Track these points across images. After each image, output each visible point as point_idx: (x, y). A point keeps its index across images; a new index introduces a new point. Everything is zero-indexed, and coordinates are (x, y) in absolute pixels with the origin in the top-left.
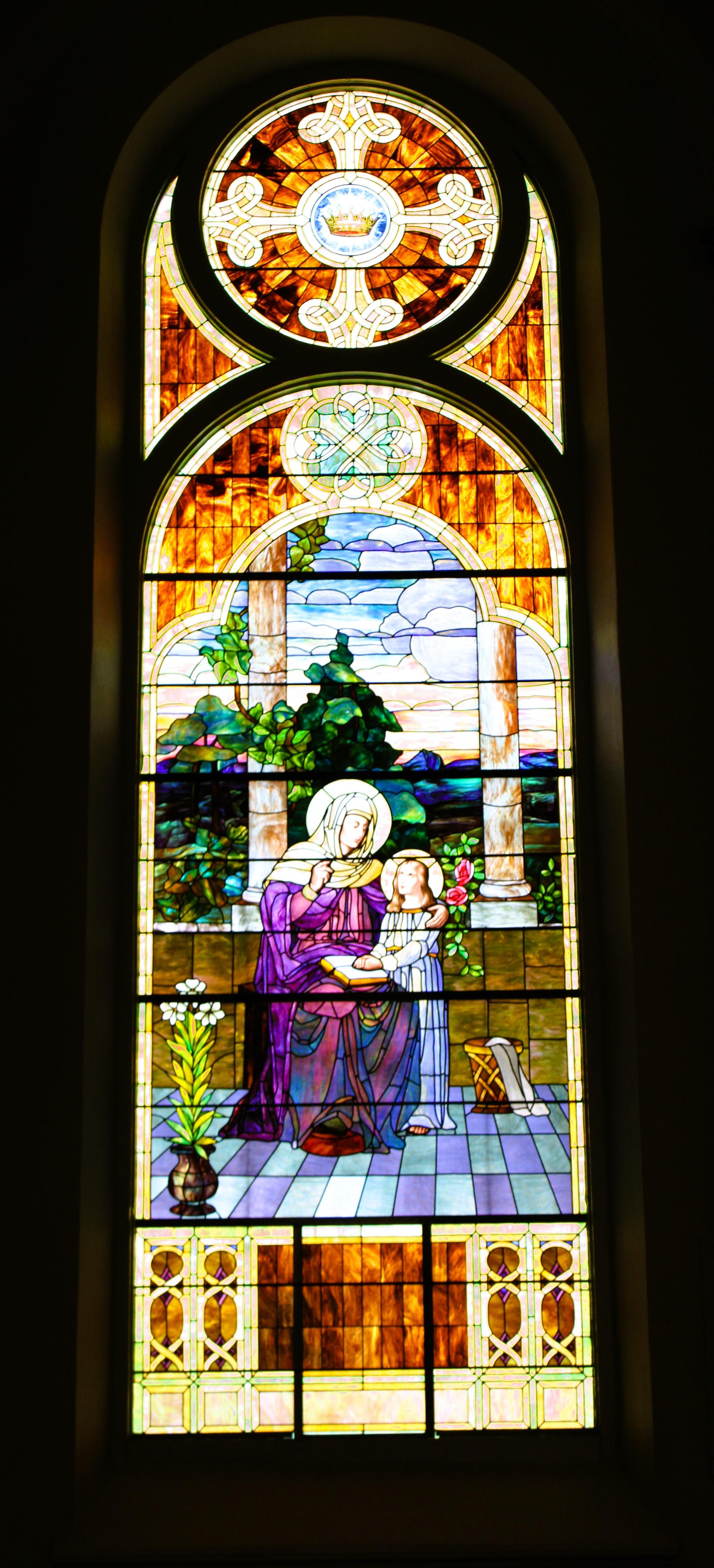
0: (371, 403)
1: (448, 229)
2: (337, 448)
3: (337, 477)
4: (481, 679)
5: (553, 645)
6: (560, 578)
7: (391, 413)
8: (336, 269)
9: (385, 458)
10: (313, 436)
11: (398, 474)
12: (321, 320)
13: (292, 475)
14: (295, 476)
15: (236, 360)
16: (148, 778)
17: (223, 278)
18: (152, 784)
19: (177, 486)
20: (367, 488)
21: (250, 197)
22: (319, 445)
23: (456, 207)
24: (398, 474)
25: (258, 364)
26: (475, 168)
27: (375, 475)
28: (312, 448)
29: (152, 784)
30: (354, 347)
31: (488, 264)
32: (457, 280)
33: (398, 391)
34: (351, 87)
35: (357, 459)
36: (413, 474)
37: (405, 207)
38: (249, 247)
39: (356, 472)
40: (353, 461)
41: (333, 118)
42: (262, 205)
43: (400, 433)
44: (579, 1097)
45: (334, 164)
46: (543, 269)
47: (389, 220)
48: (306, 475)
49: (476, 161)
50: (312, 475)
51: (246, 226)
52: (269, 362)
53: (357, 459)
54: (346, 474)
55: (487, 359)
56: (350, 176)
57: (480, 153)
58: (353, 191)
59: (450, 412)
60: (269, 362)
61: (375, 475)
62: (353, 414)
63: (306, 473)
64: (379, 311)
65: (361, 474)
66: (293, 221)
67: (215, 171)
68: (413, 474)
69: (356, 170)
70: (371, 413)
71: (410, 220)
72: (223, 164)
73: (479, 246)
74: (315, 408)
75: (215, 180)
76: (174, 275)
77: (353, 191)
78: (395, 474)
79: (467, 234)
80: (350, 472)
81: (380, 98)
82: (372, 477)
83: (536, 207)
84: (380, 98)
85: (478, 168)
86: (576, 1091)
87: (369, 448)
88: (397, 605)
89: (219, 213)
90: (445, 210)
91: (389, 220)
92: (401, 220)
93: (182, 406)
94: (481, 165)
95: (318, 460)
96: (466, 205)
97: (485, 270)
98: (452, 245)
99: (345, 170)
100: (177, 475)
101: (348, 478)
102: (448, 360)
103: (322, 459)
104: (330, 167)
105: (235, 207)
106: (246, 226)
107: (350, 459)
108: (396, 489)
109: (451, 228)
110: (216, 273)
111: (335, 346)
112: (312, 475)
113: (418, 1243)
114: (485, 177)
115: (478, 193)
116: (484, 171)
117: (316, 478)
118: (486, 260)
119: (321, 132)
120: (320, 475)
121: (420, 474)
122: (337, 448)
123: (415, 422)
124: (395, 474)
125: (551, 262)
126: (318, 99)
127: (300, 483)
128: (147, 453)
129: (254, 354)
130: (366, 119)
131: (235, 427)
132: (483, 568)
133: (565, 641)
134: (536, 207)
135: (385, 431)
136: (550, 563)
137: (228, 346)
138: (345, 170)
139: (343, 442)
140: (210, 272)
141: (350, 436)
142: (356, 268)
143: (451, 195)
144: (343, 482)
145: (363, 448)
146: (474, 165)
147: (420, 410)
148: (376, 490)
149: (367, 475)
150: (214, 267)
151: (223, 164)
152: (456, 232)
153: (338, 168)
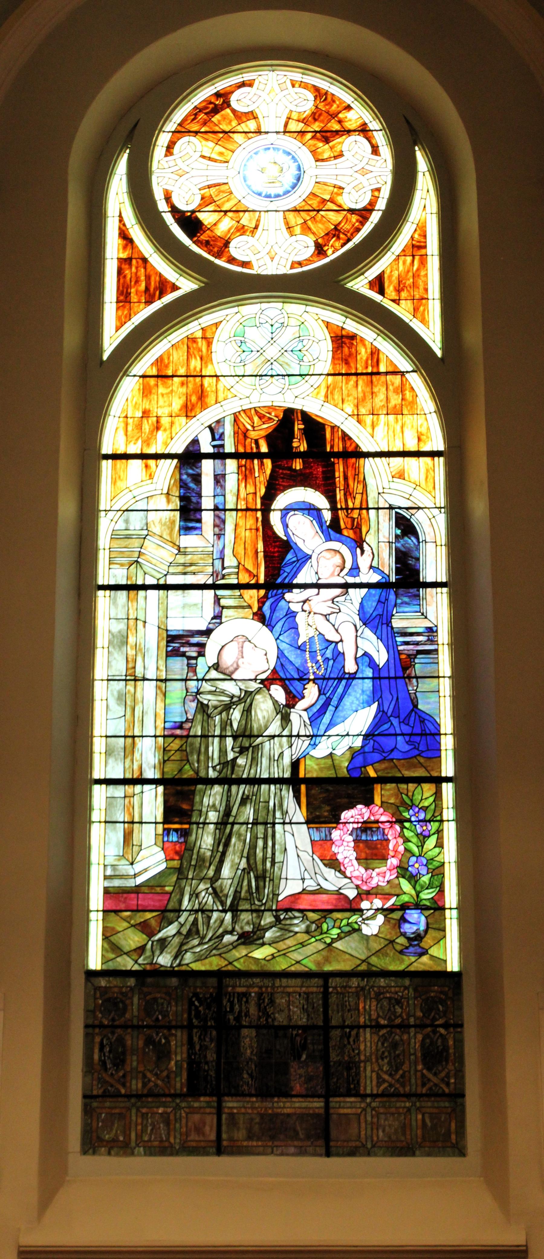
0: (286, 318)
1: (349, 179)
2: (259, 353)
3: (258, 378)
7: (302, 326)
8: (260, 212)
11: (308, 375)
12: (248, 252)
13: (222, 376)
14: (224, 376)
15: (177, 284)
17: (169, 219)
21: (353, 191)
22: (244, 351)
23: (357, 162)
24: (308, 375)
26: (372, 131)
27: (289, 375)
28: (239, 353)
33: (309, 309)
34: (274, 68)
35: (275, 363)
36: (320, 375)
37: (316, 161)
39: (274, 373)
43: (311, 342)
44: (454, 905)
45: (285, 215)
47: (302, 172)
51: (356, 168)
52: (203, 285)
53: (275, 363)
55: (379, 284)
56: (272, 137)
58: (274, 149)
59: (352, 326)
60: (203, 285)
61: (289, 375)
62: (272, 325)
64: (295, 245)
65: (278, 375)
66: (318, 172)
67: (164, 132)
68: (320, 375)
70: (285, 325)
71: (318, 172)
72: (171, 126)
74: (241, 321)
75: (163, 139)
77: (274, 149)
78: (306, 375)
79: (179, 162)
80: (269, 374)
81: (297, 76)
82: (286, 377)
83: (422, 163)
86: (451, 898)
87: (285, 353)
91: (302, 172)
92: (231, 173)
93: (133, 320)
95: (243, 364)
96: (365, 161)
97: (380, 213)
98: (192, 153)
99: (267, 133)
100: (128, 376)
102: (349, 285)
104: (287, 213)
105: (366, 183)
107: (269, 363)
108: (307, 386)
109: (353, 179)
110: (163, 214)
111: (259, 272)
113: (308, 828)
114: (380, 138)
115: (375, 150)
118: (381, 204)
119: (250, 103)
124: (306, 375)
128: (105, 357)
130: (258, 256)
134: (422, 163)
135: (298, 339)
138: (267, 133)
139: (264, 349)
140: (158, 214)
141: (270, 344)
142: (276, 211)
143: (353, 153)
145: (280, 353)
146: (372, 128)
147: (328, 325)
148: (290, 387)
149: (283, 375)
151: (171, 126)
152: (187, 163)
153: (282, 213)
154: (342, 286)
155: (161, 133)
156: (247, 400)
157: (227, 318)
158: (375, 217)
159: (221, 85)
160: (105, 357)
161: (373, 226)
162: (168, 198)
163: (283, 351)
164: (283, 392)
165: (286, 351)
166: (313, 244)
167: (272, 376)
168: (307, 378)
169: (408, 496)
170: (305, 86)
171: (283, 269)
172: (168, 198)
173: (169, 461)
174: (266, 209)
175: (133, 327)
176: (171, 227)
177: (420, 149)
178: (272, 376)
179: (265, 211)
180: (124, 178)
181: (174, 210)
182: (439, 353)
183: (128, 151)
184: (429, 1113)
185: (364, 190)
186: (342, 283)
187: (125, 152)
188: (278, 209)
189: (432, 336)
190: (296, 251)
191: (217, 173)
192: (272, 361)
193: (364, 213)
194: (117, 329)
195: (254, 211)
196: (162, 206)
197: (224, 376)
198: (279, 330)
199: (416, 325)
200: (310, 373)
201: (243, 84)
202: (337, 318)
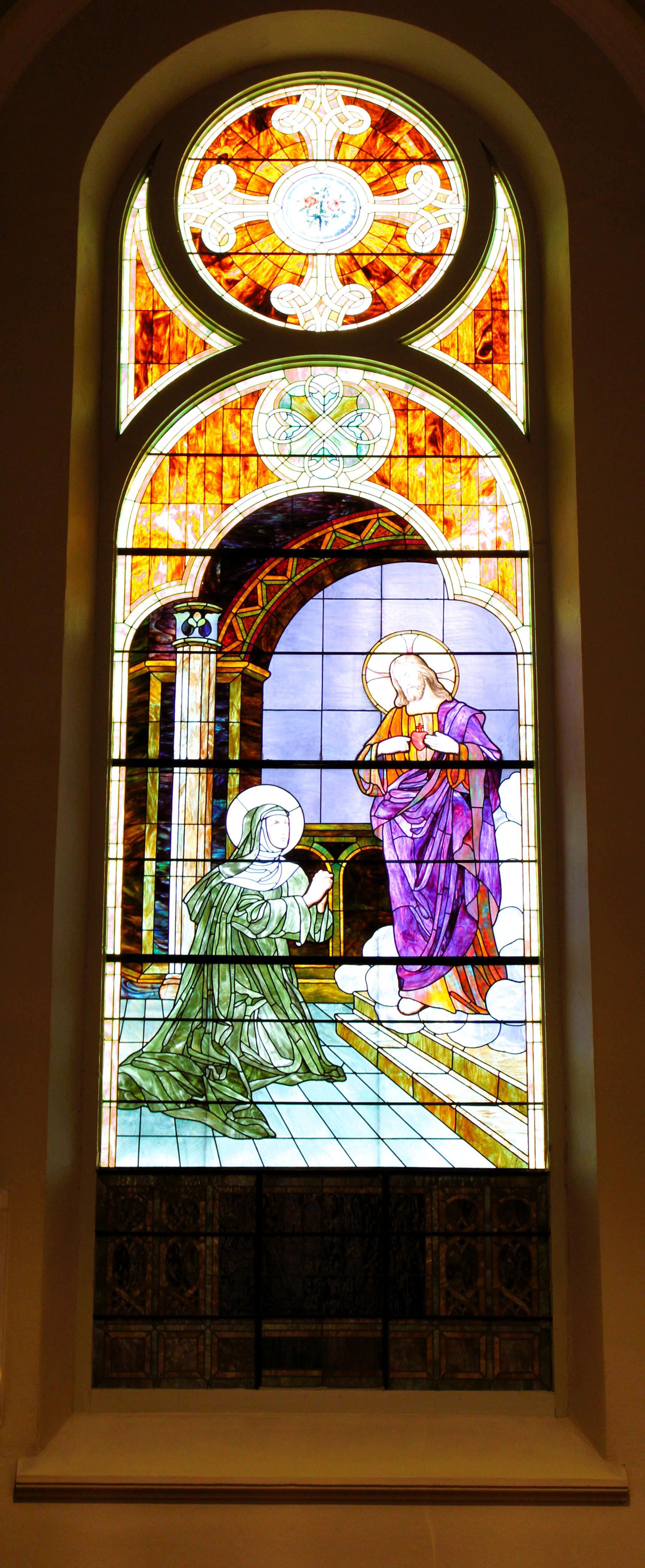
3: (307, 458)
4: (142, 1022)
5: (517, 624)
6: (523, 559)
8: (335, 160)
9: (355, 440)
10: (284, 416)
11: (366, 456)
14: (275, 455)
16: (118, 763)
17: (197, 261)
18: (176, 757)
19: (146, 466)
20: (312, 384)
24: (366, 456)
25: (230, 346)
29: (176, 757)
30: (324, 330)
31: (454, 252)
32: (417, 426)
35: (327, 440)
38: (419, 184)
39: (326, 453)
40: (324, 441)
41: (305, 110)
42: (236, 193)
46: (510, 256)
48: (278, 456)
49: (443, 153)
50: (284, 456)
54: (315, 456)
57: (446, 142)
63: (278, 453)
64: (349, 296)
65: (332, 456)
67: (190, 159)
69: (326, 160)
70: (341, 395)
71: (264, 208)
73: (446, 234)
75: (189, 169)
76: (151, 260)
80: (321, 453)
81: (351, 92)
82: (341, 459)
84: (351, 92)
85: (446, 160)
88: (507, 979)
89: (193, 199)
90: (412, 199)
94: (449, 158)
96: (434, 195)
97: (452, 258)
100: (149, 454)
101: (317, 459)
102: (416, 345)
103: (293, 440)
106: (221, 212)
108: (365, 469)
110: (190, 256)
111: (305, 328)
112: (284, 456)
114: (453, 169)
116: (452, 163)
117: (286, 458)
118: (453, 247)
120: (290, 456)
121: (387, 457)
122: (308, 429)
123: (383, 406)
125: (515, 253)
126: (292, 91)
127: (271, 463)
128: (123, 428)
129: (225, 335)
130: (304, 309)
131: (207, 407)
132: (449, 549)
133: (528, 620)
136: (513, 545)
137: (202, 331)
138: (317, 160)
141: (327, 435)
144: (313, 462)
147: (390, 395)
148: (345, 470)
149: (336, 456)
150: (188, 251)
151: (198, 151)
152: (423, 221)
154: (406, 348)
155: (187, 161)
156: (294, 486)
157: (271, 386)
158: (444, 264)
159: (261, 102)
160: (123, 428)
161: (442, 273)
162: (197, 236)
163: (311, 426)
164: (336, 476)
165: (307, 426)
166: (370, 296)
167: (324, 456)
168: (365, 459)
169: (483, 605)
170: (364, 104)
171: (335, 325)
172: (197, 236)
173: (199, 559)
174: (314, 252)
175: (155, 394)
176: (200, 273)
177: (500, 182)
178: (324, 456)
179: (329, 160)
180: (510, 212)
181: (203, 251)
182: (522, 428)
183: (147, 180)
184: (203, 1318)
185: (431, 231)
186: (406, 342)
187: (144, 182)
188: (329, 252)
189: (514, 409)
190: (349, 303)
191: (388, 206)
192: (324, 438)
193: (430, 259)
194: (137, 395)
195: (300, 254)
196: (190, 246)
197: (275, 455)
198: (333, 401)
199: (496, 395)
200: (369, 454)
201: (288, 100)
202: (398, 384)
